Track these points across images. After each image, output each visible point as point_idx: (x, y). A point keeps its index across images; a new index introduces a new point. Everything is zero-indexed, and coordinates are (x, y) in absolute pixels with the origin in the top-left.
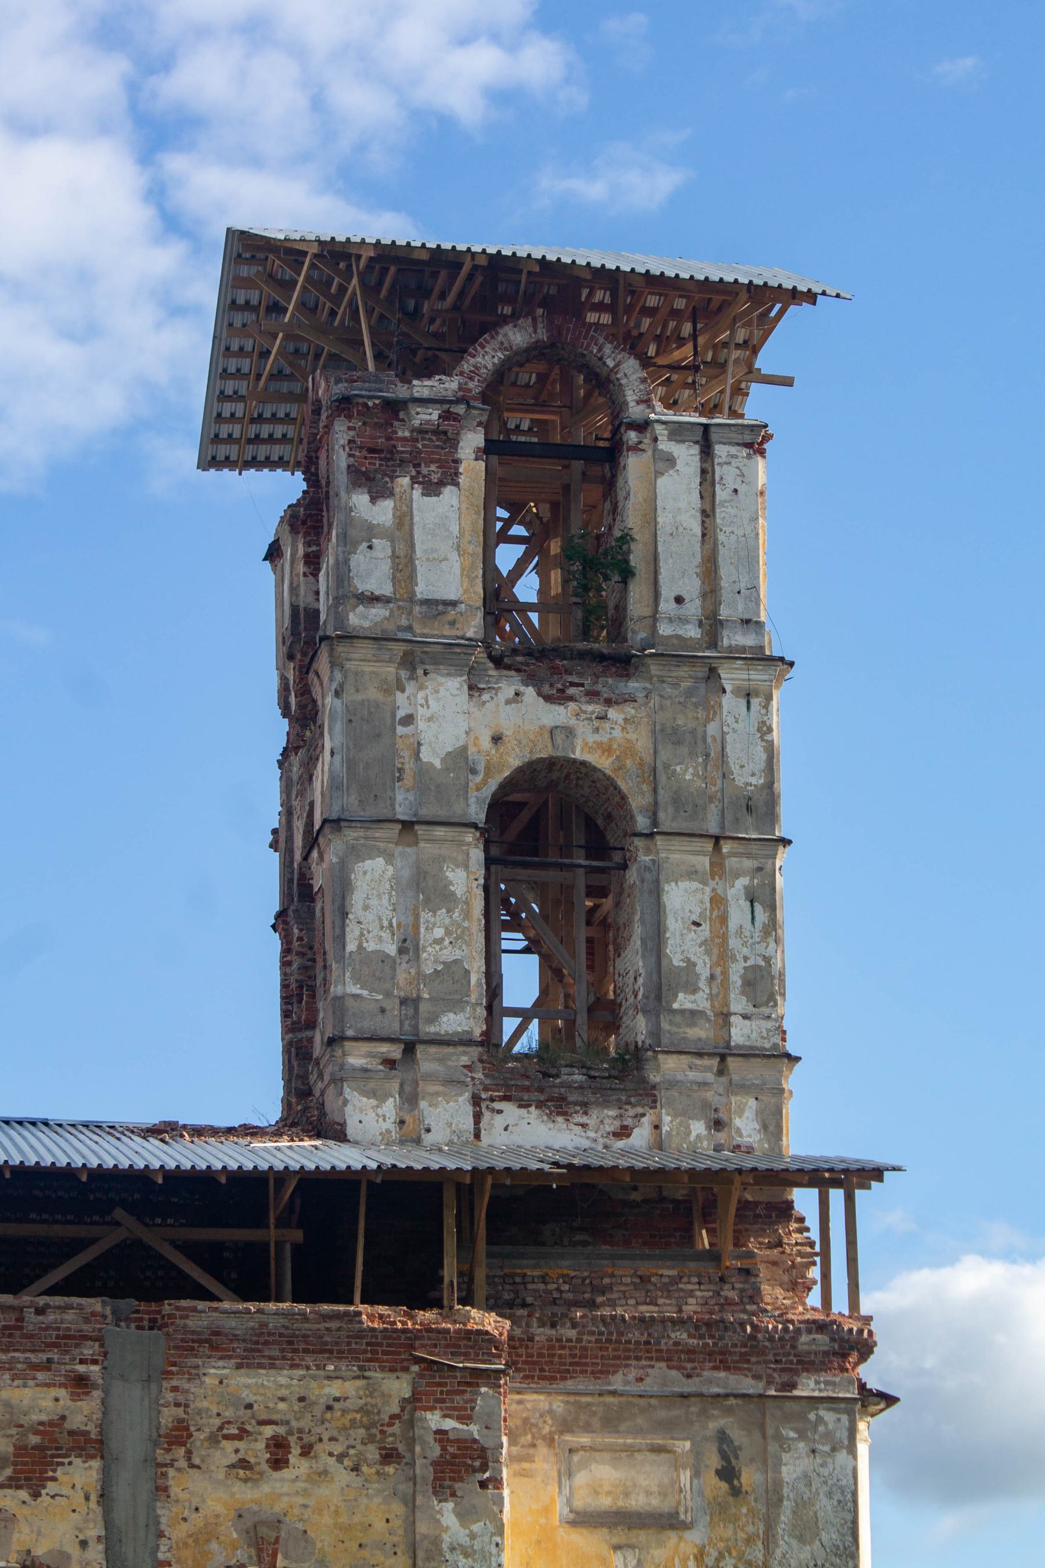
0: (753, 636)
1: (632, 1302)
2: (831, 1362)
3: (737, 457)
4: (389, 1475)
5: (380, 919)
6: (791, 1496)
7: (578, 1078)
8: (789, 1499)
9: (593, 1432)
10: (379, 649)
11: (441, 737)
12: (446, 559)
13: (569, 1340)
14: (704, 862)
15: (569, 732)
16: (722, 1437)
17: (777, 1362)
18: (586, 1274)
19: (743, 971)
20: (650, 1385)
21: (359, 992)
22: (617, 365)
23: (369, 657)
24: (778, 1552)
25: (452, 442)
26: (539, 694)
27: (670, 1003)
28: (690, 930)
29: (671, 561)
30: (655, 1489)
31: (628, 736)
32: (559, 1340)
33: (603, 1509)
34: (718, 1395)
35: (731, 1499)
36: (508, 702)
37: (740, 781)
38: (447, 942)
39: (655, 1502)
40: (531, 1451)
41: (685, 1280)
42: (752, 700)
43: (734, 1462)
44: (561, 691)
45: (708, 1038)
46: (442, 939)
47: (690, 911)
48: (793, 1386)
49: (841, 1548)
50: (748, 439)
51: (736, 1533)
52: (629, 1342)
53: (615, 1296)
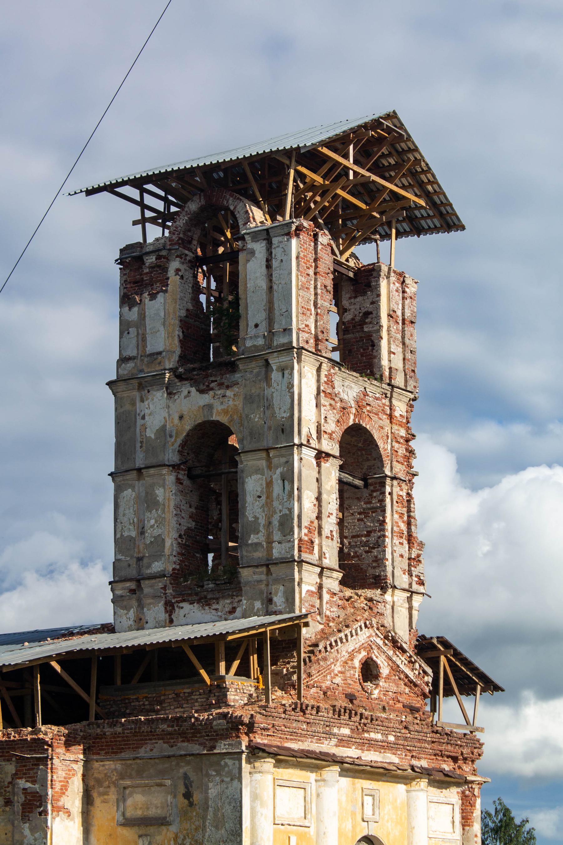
0: (288, 337)
1: (172, 707)
2: (231, 733)
3: (282, 242)
4: (7, 812)
5: (130, 520)
6: (213, 806)
7: (211, 586)
8: (211, 807)
9: (132, 778)
10: (128, 384)
11: (154, 422)
12: (159, 331)
13: (119, 733)
14: (264, 463)
15: (210, 407)
16: (186, 776)
17: (208, 736)
18: (154, 695)
19: (279, 518)
20: (156, 753)
21: (121, 557)
22: (235, 208)
23: (125, 389)
24: (207, 834)
25: (165, 270)
26: (197, 390)
27: (247, 541)
28: (256, 500)
29: (253, 306)
30: (159, 805)
31: (235, 403)
32: (116, 734)
33: (138, 816)
34: (181, 756)
35: (189, 808)
36: (185, 397)
37: (278, 416)
38: (156, 526)
39: (159, 811)
40: (108, 790)
41: (194, 694)
42: (285, 372)
43: (190, 789)
44: (208, 386)
45: (263, 556)
46: (154, 525)
47: (257, 491)
48: (214, 747)
49: (235, 831)
50: (286, 231)
51: (191, 826)
52: (143, 732)
53: (166, 705)
